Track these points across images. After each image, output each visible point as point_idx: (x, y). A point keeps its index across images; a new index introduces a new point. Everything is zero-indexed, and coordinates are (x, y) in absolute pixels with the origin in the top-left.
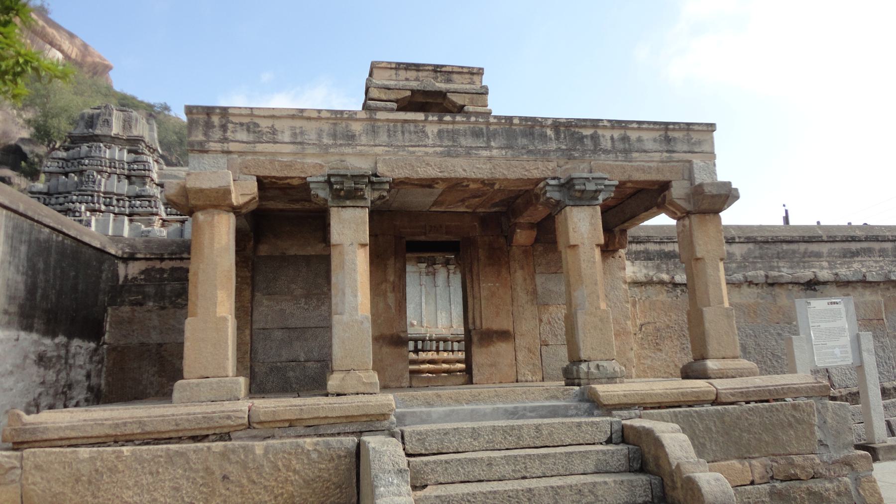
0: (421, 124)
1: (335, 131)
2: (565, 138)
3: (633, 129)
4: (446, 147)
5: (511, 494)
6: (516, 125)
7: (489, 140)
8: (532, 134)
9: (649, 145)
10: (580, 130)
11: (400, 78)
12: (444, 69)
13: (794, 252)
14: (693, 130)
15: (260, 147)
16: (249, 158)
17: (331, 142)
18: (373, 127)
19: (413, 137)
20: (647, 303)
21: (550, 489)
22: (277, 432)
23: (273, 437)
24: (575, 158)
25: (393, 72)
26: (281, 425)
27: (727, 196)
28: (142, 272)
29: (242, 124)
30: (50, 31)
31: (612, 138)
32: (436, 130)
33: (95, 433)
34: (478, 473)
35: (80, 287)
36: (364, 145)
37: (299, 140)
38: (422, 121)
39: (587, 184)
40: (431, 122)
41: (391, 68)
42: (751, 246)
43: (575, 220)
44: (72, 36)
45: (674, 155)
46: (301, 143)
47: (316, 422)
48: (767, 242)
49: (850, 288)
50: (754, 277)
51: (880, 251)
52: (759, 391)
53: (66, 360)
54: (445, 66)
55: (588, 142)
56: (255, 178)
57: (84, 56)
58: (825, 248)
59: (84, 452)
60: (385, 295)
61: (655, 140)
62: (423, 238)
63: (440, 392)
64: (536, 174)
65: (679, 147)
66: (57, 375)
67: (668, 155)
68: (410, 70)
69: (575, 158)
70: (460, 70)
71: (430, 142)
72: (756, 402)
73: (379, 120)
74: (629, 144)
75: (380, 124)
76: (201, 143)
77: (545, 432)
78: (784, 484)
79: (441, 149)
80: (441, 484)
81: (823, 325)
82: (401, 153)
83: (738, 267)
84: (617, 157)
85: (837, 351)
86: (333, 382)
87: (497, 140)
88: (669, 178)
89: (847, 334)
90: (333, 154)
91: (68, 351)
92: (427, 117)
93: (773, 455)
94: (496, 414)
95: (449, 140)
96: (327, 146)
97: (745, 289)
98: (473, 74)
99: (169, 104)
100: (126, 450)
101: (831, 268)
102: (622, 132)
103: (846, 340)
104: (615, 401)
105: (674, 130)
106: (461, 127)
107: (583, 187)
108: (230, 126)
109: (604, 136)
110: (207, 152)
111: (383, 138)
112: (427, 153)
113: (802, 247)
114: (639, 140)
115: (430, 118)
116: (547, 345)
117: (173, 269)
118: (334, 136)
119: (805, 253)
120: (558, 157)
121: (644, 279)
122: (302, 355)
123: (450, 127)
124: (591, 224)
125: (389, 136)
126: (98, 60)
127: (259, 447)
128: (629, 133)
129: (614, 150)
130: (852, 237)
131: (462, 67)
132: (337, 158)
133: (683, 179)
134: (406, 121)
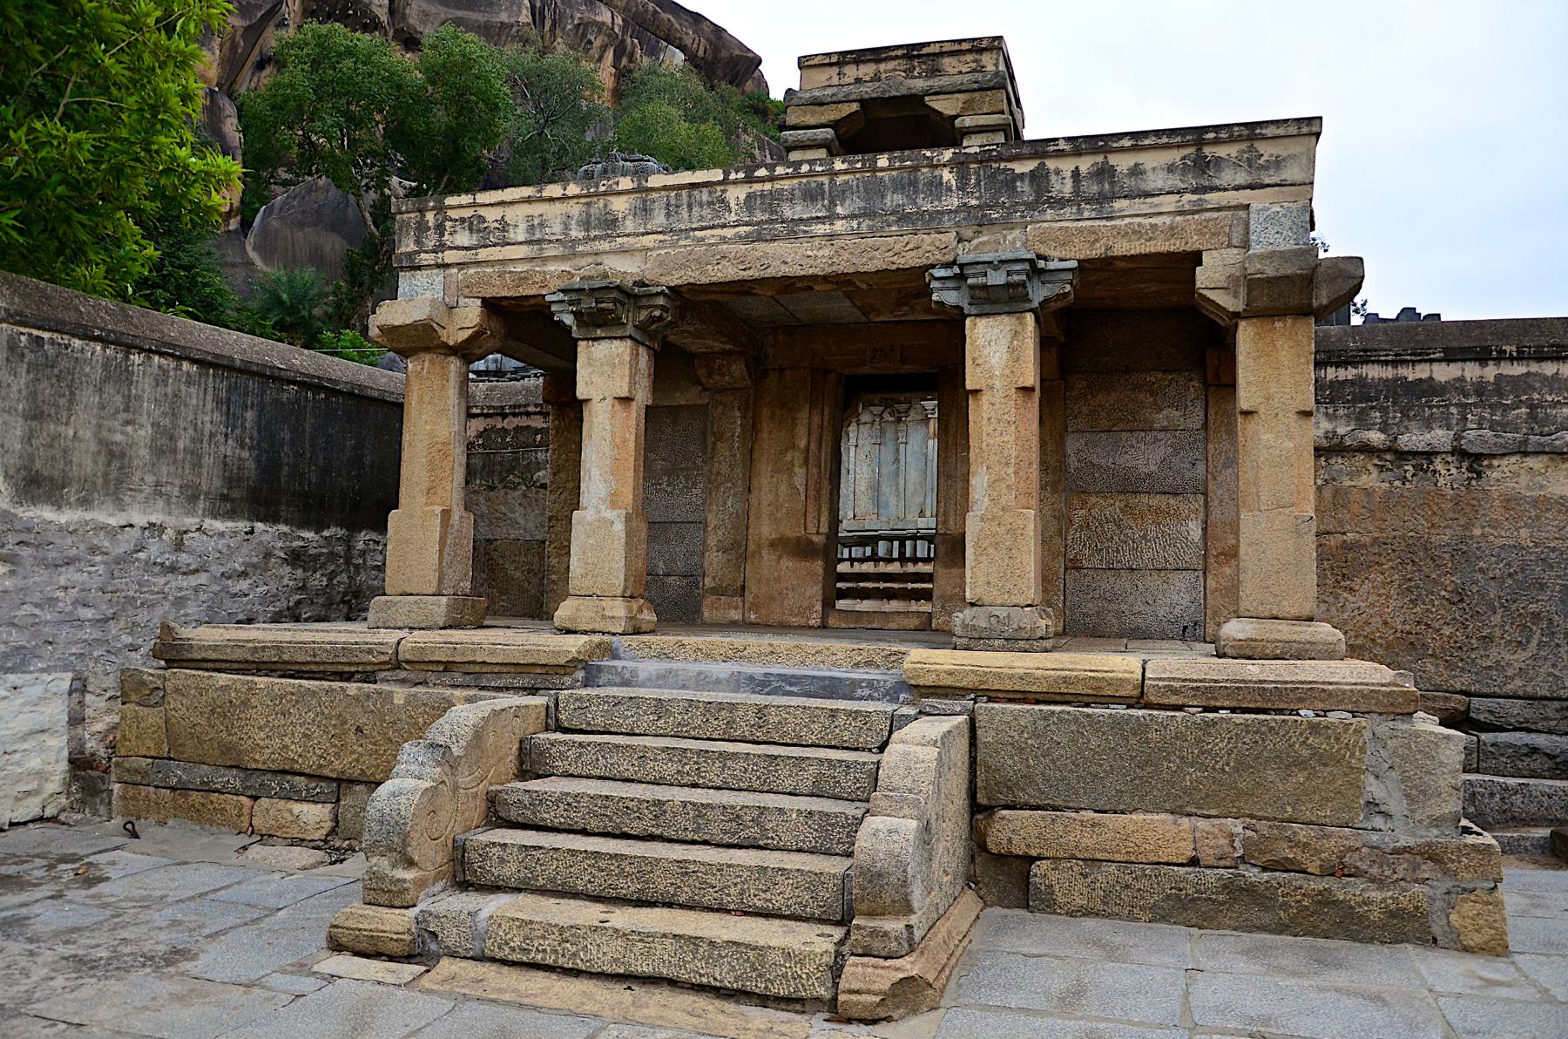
0: (719, 188)
1: (588, 215)
2: (978, 183)
3: (1122, 150)
4: (758, 224)
5: (631, 804)
6: (882, 170)
7: (833, 204)
8: (913, 183)
9: (1156, 181)
10: (1009, 166)
11: (846, 80)
12: (925, 51)
14: (1264, 138)
15: (483, 254)
16: (472, 271)
17: (581, 235)
18: (644, 201)
19: (706, 212)
21: (689, 807)
22: (432, 678)
23: (425, 683)
24: (992, 223)
25: (835, 70)
26: (434, 667)
27: (1350, 274)
28: (480, 435)
29: (463, 220)
31: (1076, 173)
32: (742, 197)
33: (234, 657)
34: (626, 767)
35: (368, 461)
36: (628, 235)
37: (538, 236)
38: (719, 183)
39: (990, 272)
40: (735, 182)
41: (831, 65)
43: (980, 342)
45: (1207, 196)
46: (539, 242)
47: (477, 668)
52: (1259, 688)
53: (348, 562)
54: (928, 44)
55: (1024, 187)
56: (479, 302)
57: (716, 50)
59: (223, 679)
60: (790, 471)
61: (1171, 169)
62: (865, 370)
63: (686, 640)
64: (912, 260)
66: (330, 580)
67: (1195, 197)
68: (864, 62)
69: (992, 223)
70: (957, 47)
71: (733, 217)
72: (1233, 710)
73: (652, 189)
74: (1112, 183)
75: (655, 195)
76: (410, 255)
77: (773, 719)
78: (1266, 876)
79: (747, 229)
80: (572, 775)
82: (682, 243)
84: (1080, 211)
86: (564, 611)
87: (848, 202)
88: (1197, 246)
90: (583, 255)
91: (349, 548)
92: (727, 174)
93: (1252, 816)
94: (736, 682)
95: (763, 211)
96: (576, 241)
98: (981, 51)
100: (262, 681)
102: (1100, 159)
104: (930, 680)
105: (1217, 142)
107: (982, 280)
108: (448, 224)
109: (1058, 172)
110: (419, 268)
111: (659, 219)
112: (723, 240)
114: (1136, 171)
115: (733, 176)
116: (1078, 569)
117: (517, 429)
118: (586, 224)
120: (957, 224)
122: (661, 565)
123: (768, 186)
124: (1011, 350)
125: (668, 215)
127: (400, 694)
128: (1114, 159)
129: (1077, 199)
131: (960, 41)
132: (590, 259)
133: (1230, 246)
134: (693, 186)
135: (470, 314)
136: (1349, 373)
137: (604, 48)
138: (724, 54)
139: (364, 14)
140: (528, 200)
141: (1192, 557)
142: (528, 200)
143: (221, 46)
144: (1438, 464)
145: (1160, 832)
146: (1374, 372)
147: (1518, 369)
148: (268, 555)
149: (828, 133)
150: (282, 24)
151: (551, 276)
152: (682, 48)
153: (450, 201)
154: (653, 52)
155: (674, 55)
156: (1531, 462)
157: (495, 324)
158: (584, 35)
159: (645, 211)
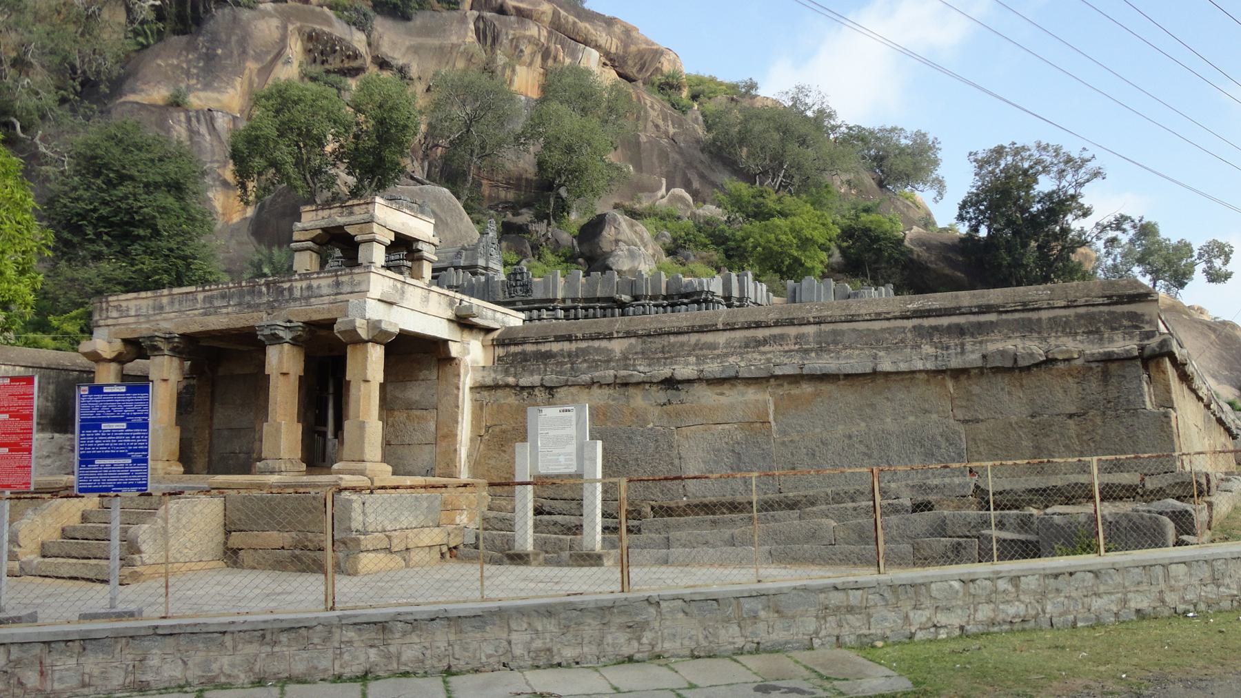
9: (325, 291)
13: (682, 345)
15: (121, 321)
20: (495, 407)
30: (583, 25)
42: (633, 340)
44: (610, 22)
48: (649, 335)
49: (726, 386)
50: (601, 377)
51: (796, 338)
57: (626, 46)
58: (721, 338)
65: (346, 289)
81: (552, 433)
83: (589, 367)
85: (562, 458)
89: (574, 441)
97: (596, 390)
99: (754, 80)
101: (697, 364)
103: (572, 448)
106: (215, 293)
113: (694, 338)
114: (319, 287)
118: (154, 309)
119: (696, 345)
121: (492, 384)
126: (644, 46)
130: (756, 323)
135: (118, 346)
136: (518, 349)
137: (533, 54)
138: (633, 48)
139: (348, 48)
140: (136, 299)
141: (431, 439)
142: (136, 299)
143: (242, 83)
144: (537, 392)
145: (275, 538)
146: (529, 348)
147: (583, 345)
148: (61, 448)
149: (310, 244)
150: (288, 62)
151: (142, 329)
152: (597, 47)
153: (110, 299)
154: (573, 54)
155: (590, 54)
156: (572, 389)
157: (129, 348)
158: (517, 47)
159: (172, 303)
